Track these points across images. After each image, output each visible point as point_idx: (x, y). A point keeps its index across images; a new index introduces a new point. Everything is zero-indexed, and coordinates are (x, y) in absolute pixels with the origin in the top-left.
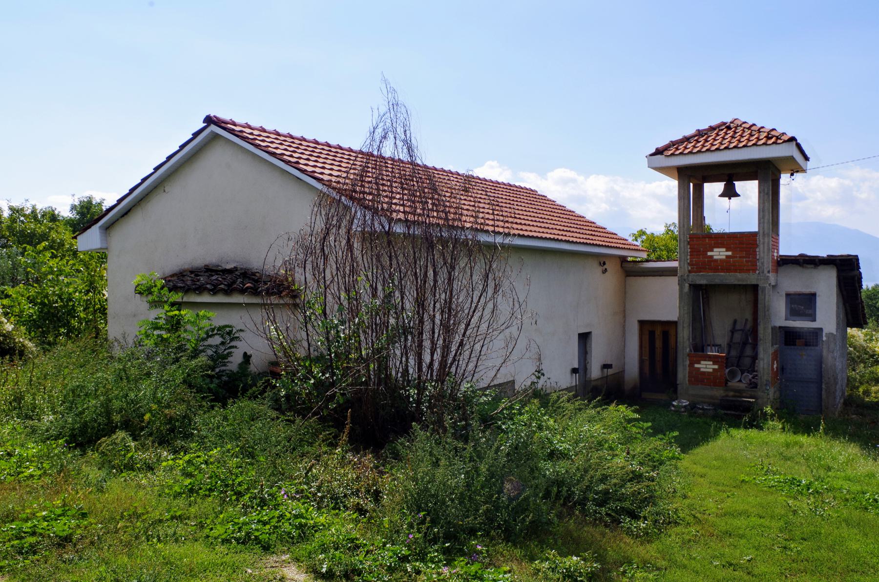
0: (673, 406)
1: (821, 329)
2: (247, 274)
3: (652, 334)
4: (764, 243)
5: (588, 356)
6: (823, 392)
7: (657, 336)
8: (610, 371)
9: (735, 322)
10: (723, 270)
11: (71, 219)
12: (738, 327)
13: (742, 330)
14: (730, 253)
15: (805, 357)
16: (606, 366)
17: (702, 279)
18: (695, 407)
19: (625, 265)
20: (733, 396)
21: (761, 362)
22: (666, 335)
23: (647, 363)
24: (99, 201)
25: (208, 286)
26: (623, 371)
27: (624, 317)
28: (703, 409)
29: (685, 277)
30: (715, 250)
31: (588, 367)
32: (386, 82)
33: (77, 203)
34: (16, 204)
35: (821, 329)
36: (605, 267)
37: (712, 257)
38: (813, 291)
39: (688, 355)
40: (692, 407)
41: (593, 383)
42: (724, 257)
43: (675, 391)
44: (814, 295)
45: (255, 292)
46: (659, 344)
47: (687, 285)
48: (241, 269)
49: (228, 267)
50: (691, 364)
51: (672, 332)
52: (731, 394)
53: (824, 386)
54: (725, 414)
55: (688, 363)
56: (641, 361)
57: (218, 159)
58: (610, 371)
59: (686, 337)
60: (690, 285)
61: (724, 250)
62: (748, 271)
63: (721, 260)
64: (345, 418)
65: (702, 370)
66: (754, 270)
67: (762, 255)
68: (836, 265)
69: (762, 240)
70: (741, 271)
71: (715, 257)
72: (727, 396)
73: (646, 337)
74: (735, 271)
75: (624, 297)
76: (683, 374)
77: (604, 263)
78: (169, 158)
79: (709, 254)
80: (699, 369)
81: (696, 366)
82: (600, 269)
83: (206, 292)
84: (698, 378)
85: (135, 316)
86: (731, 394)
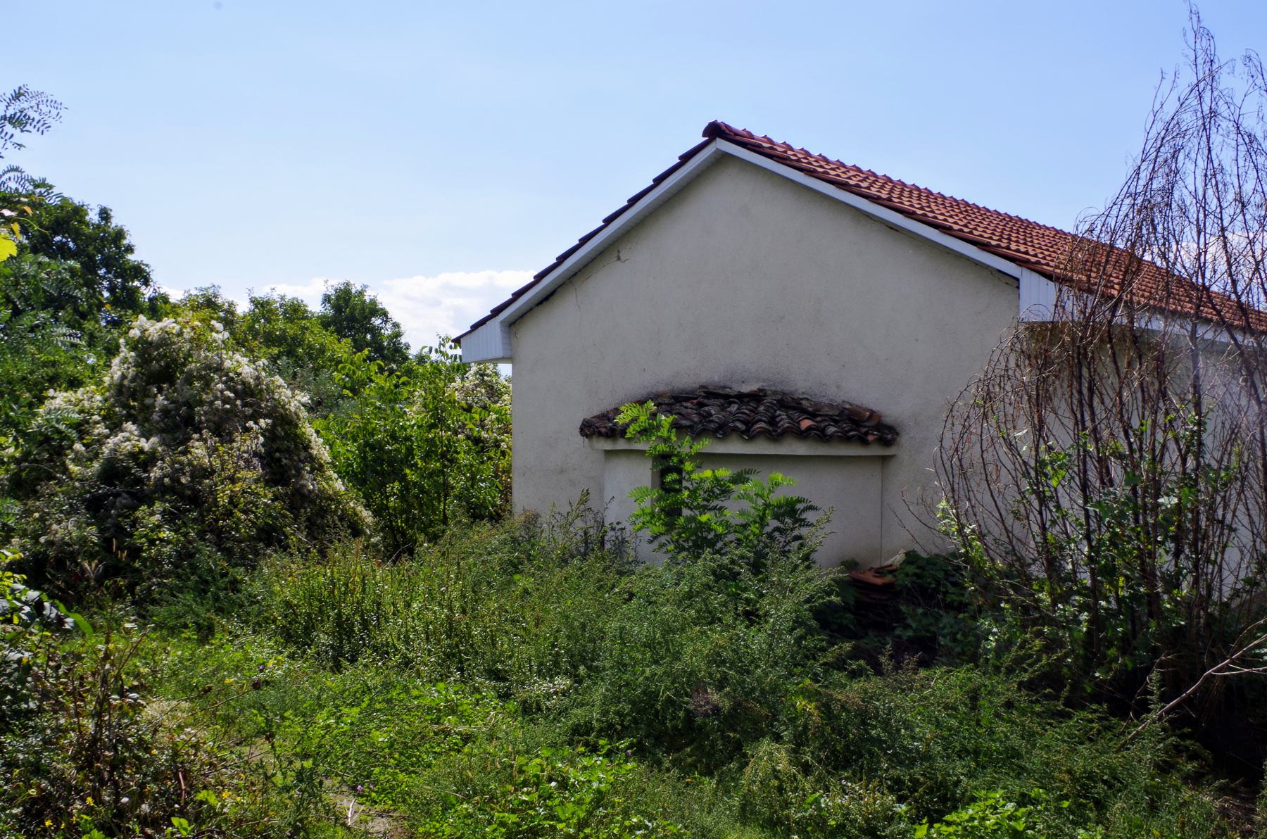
2: (791, 403)
11: (324, 316)
24: (359, 289)
25: (739, 425)
32: (1195, 14)
33: (331, 292)
34: (262, 293)
45: (821, 436)
48: (775, 393)
49: (746, 389)
57: (725, 198)
64: (1183, 701)
78: (633, 201)
83: (734, 436)
85: (562, 471)
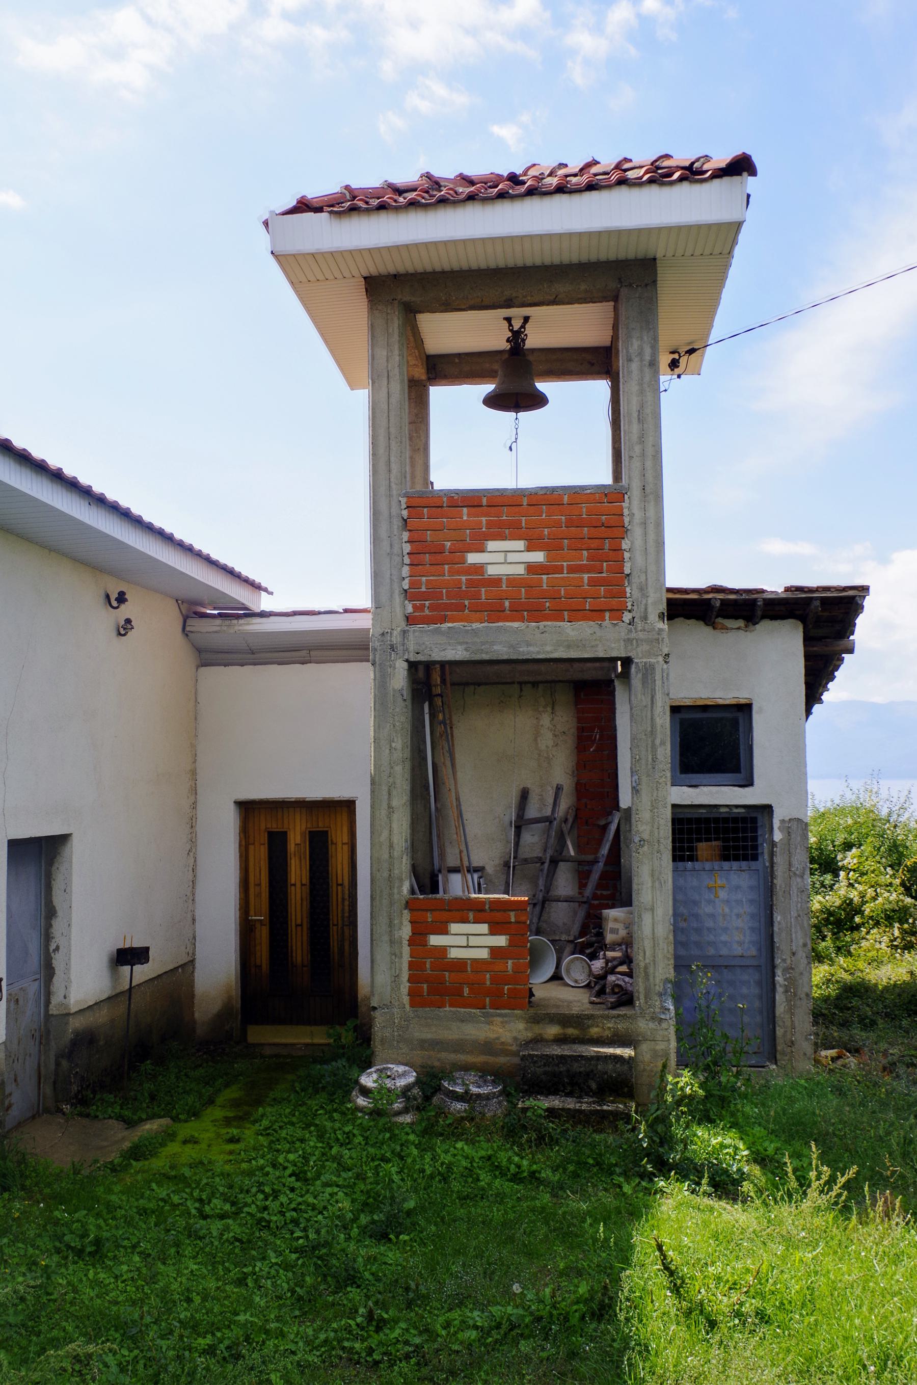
0: (365, 1092)
1: (768, 809)
3: (277, 843)
4: (644, 524)
5: (58, 926)
6: (780, 997)
7: (292, 847)
8: (142, 972)
9: (524, 795)
10: (518, 612)
12: (532, 812)
13: (549, 820)
14: (538, 557)
15: (723, 894)
16: (129, 956)
17: (448, 644)
18: (438, 1089)
19: (197, 625)
20: (561, 1040)
21: (647, 919)
22: (319, 844)
23: (263, 934)
26: (189, 965)
27: (194, 791)
28: (465, 1097)
29: (396, 638)
30: (492, 545)
31: (58, 961)
35: (768, 809)
36: (126, 611)
37: (479, 569)
38: (726, 694)
39: (408, 905)
40: (430, 1083)
41: (76, 1024)
42: (520, 570)
43: (364, 1036)
44: (745, 709)
46: (298, 871)
47: (401, 667)
50: (418, 937)
51: (339, 836)
52: (553, 1031)
53: (779, 979)
54: (552, 1113)
55: (406, 931)
56: (247, 930)
58: (142, 972)
59: (293, 862)
60: (413, 666)
61: (520, 545)
62: (597, 614)
63: (513, 581)
65: (454, 954)
66: (617, 612)
67: (639, 560)
68: (803, 619)
69: (638, 515)
70: (577, 614)
71: (492, 571)
72: (538, 1040)
73: (260, 853)
74: (556, 615)
75: (191, 726)
76: (381, 969)
77: (121, 598)
79: (473, 558)
80: (444, 950)
81: (435, 940)
82: (110, 618)
84: (437, 984)
86: (553, 1031)
